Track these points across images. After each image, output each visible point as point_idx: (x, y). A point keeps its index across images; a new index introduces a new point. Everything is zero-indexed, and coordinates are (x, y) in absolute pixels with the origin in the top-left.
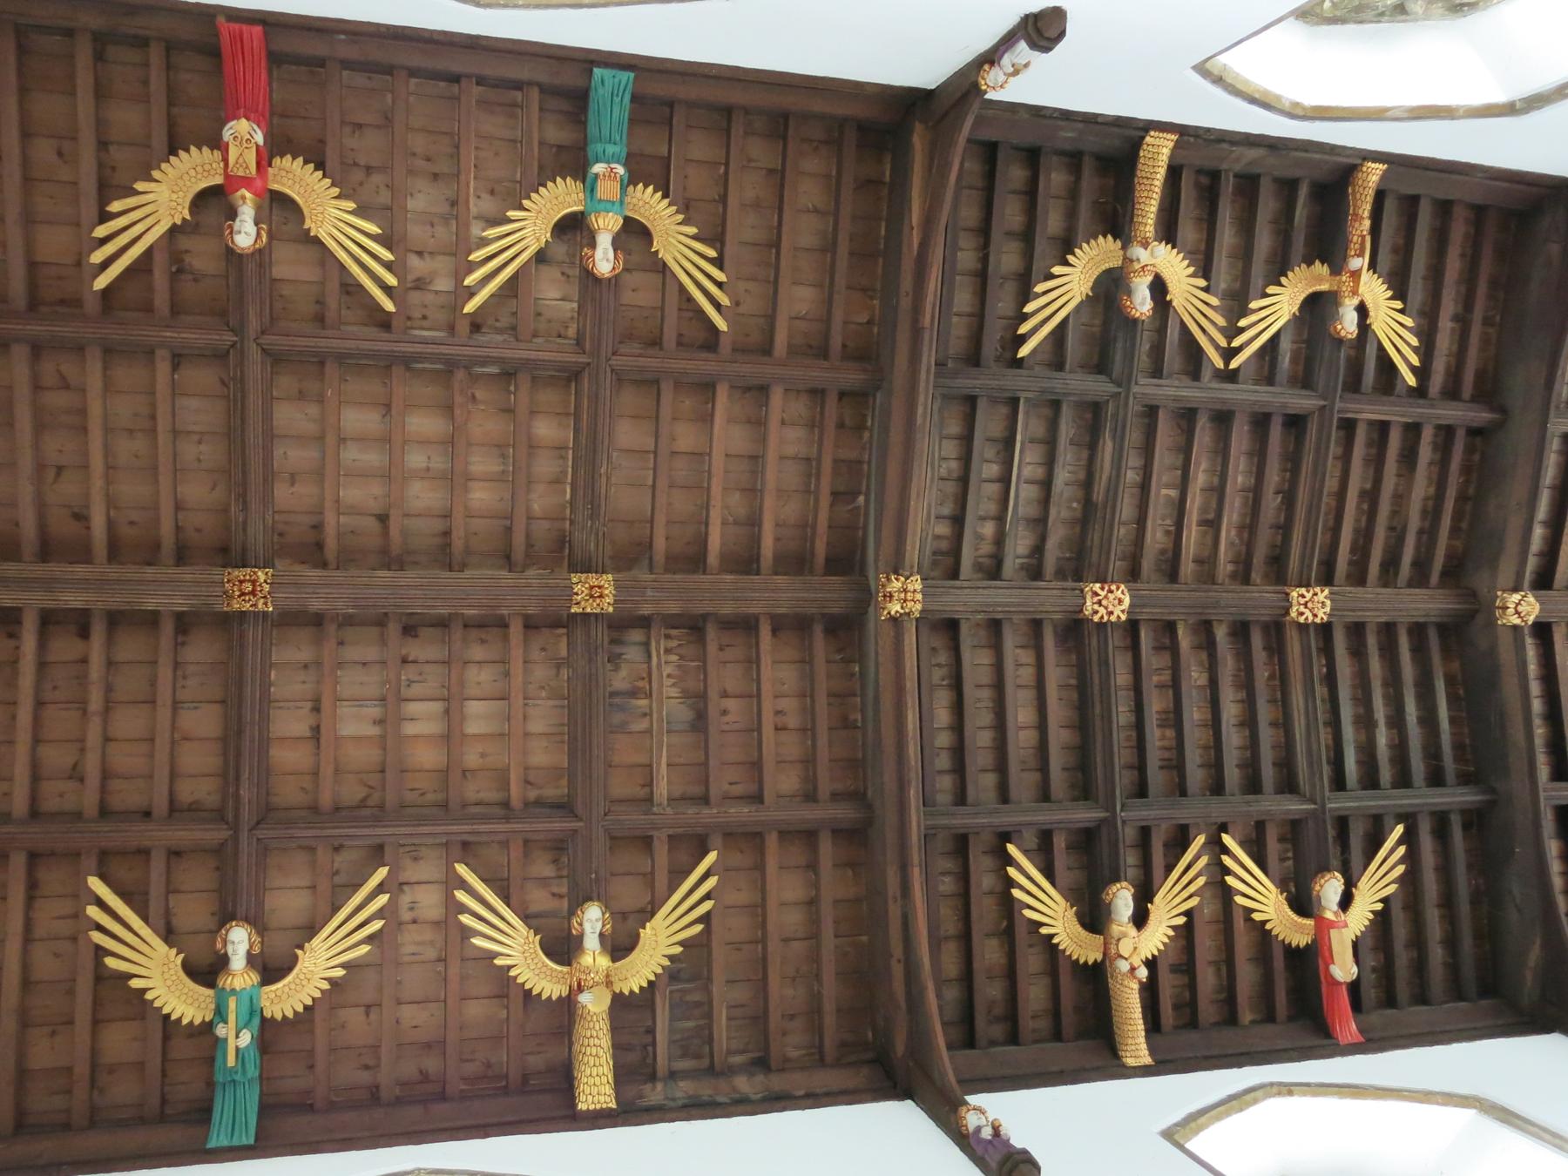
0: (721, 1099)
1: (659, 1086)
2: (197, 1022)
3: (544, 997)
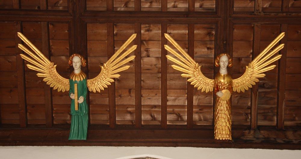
0: (279, 141)
1: (252, 132)
2: (63, 91)
3: (202, 91)
